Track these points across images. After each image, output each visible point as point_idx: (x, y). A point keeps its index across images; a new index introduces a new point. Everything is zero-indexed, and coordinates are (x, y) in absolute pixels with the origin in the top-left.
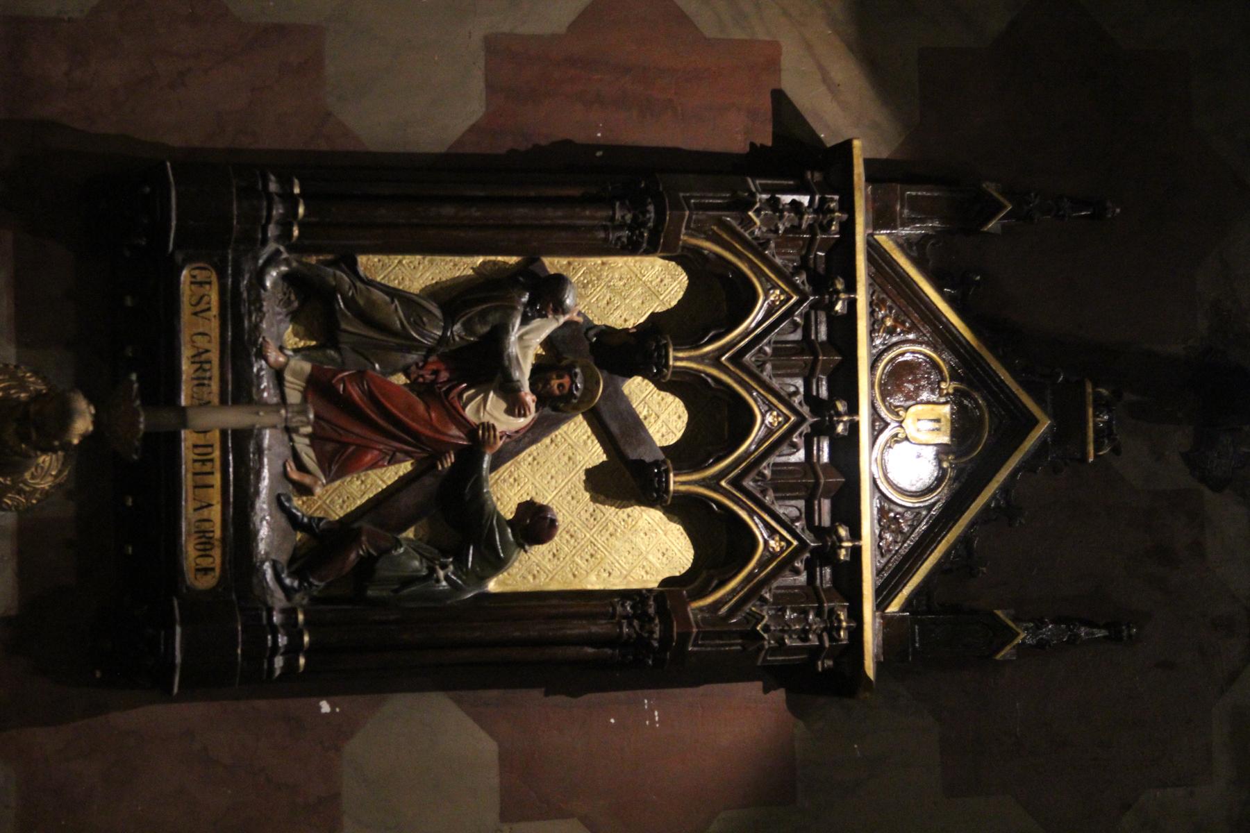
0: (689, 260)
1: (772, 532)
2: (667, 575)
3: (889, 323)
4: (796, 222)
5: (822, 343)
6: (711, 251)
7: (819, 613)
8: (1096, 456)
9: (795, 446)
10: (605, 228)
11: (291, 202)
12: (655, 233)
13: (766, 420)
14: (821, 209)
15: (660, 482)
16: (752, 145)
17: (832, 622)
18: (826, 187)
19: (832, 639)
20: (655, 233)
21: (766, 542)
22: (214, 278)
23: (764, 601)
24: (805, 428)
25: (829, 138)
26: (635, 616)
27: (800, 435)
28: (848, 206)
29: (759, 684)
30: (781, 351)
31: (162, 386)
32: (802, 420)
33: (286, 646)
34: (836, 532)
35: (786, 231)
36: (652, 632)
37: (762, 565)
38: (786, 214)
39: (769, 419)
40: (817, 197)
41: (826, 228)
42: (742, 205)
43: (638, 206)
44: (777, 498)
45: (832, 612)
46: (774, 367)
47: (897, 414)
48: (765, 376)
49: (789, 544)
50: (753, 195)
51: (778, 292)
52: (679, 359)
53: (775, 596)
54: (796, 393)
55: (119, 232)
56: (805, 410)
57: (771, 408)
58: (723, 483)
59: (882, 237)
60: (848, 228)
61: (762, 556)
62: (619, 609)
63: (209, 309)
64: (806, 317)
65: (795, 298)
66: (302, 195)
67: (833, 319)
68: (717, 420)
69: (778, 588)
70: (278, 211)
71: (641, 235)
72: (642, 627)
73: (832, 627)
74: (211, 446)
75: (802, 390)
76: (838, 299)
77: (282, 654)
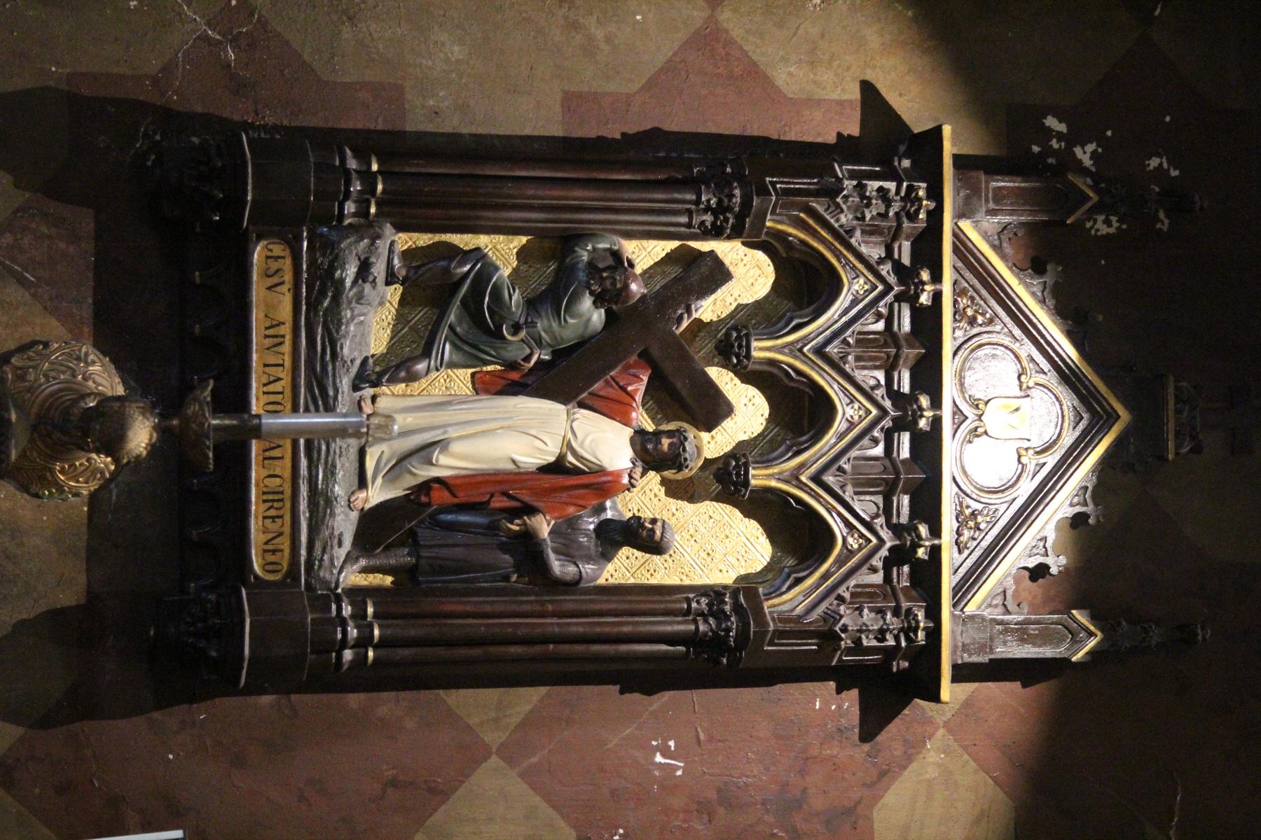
0: (771, 246)
1: (852, 400)
2: (743, 572)
3: (970, 312)
4: (882, 210)
5: (904, 462)
6: (795, 237)
7: (896, 613)
8: (1177, 454)
9: (875, 441)
10: (690, 213)
11: (368, 178)
12: (741, 218)
13: (848, 411)
14: (910, 196)
15: (738, 475)
16: (839, 135)
17: (909, 622)
18: (915, 174)
19: (908, 639)
20: (741, 218)
21: (844, 539)
22: (287, 253)
23: (841, 599)
24: (887, 423)
25: (919, 126)
26: (712, 613)
27: (882, 429)
28: (936, 193)
29: (832, 684)
30: (864, 340)
31: (234, 397)
32: (888, 288)
33: (351, 661)
34: (917, 400)
35: (872, 218)
36: (728, 630)
37: (840, 562)
38: (874, 202)
39: (850, 412)
40: (905, 184)
41: (913, 217)
42: (830, 192)
43: (722, 185)
44: (856, 493)
45: (909, 611)
46: (858, 359)
47: (977, 407)
48: (847, 368)
49: (868, 412)
50: (840, 180)
51: (862, 281)
52: (761, 349)
53: (853, 595)
54: (878, 386)
55: (192, 217)
56: (887, 404)
57: (852, 400)
58: (803, 478)
59: (966, 225)
60: (936, 216)
61: (839, 555)
62: (694, 605)
63: (282, 283)
64: (890, 307)
65: (880, 288)
66: (376, 615)
67: (917, 312)
68: (799, 411)
69: (856, 586)
70: (357, 187)
71: (726, 220)
72: (719, 625)
73: (910, 627)
74: (283, 336)
75: (883, 382)
76: (923, 290)
77: (355, 202)
